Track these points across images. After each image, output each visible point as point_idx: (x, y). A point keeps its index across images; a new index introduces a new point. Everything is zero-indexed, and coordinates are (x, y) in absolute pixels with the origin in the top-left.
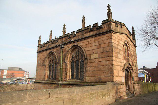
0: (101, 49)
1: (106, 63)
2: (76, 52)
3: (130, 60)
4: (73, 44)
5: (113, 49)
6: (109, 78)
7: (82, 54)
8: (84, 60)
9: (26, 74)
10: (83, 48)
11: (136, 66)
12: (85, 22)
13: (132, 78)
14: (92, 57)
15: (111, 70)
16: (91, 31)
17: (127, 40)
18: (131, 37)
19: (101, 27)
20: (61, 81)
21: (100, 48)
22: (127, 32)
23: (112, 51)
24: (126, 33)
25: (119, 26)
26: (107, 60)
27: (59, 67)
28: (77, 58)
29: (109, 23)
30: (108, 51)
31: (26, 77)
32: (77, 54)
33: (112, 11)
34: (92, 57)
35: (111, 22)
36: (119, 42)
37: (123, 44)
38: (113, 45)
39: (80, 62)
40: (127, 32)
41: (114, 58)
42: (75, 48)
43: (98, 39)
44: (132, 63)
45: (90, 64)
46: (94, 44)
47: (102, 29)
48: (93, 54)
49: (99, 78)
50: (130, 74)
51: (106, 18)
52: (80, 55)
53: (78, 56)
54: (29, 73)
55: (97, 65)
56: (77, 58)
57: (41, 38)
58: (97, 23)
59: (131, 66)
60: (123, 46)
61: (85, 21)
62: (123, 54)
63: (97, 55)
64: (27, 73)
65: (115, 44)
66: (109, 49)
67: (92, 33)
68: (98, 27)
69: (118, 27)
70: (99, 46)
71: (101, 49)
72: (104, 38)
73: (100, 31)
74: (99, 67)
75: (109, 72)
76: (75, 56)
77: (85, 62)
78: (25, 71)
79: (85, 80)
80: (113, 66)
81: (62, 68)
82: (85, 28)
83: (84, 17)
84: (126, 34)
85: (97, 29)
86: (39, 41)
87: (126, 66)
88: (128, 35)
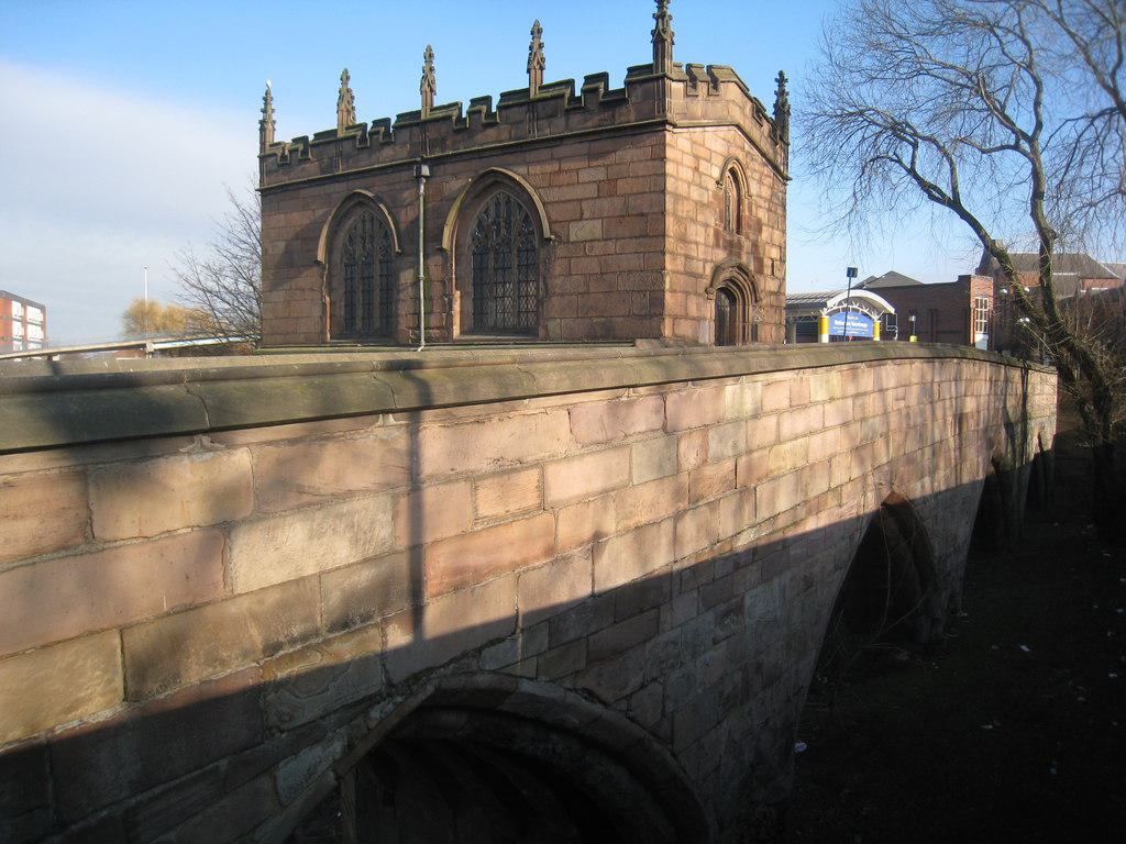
0: (618, 202)
1: (634, 262)
2: (497, 204)
3: (747, 245)
4: (480, 166)
5: (669, 206)
6: (647, 322)
7: (527, 216)
8: (536, 244)
9: (24, 322)
10: (536, 188)
11: (777, 273)
12: (543, 59)
13: (749, 330)
14: (577, 232)
15: (653, 291)
16: (575, 109)
17: (741, 156)
18: (761, 133)
19: (617, 100)
20: (423, 342)
21: (610, 196)
22: (742, 115)
23: (663, 213)
24: (740, 119)
25: (702, 89)
26: (642, 250)
27: (406, 277)
28: (503, 231)
29: (658, 87)
30: (645, 211)
31: (24, 339)
32: (503, 213)
33: (673, 26)
34: (577, 232)
35: (667, 81)
36: (696, 169)
37: (716, 173)
38: (670, 184)
39: (519, 250)
40: (742, 109)
41: (670, 243)
42: (490, 182)
43: (606, 153)
44: (759, 261)
45: (565, 262)
46: (584, 176)
47: (624, 110)
48: (581, 219)
49: (604, 324)
50: (744, 308)
51: (646, 58)
52: (518, 217)
53: (508, 222)
54: (42, 309)
55: (598, 270)
56: (503, 231)
57: (274, 105)
58: (604, 77)
59: (747, 274)
60: (718, 183)
61: (545, 52)
62: (712, 221)
63: (598, 224)
64: (34, 314)
65: (677, 179)
66: (651, 205)
67: (578, 124)
68: (607, 93)
69: (700, 98)
70: (607, 188)
71: (616, 200)
72: (631, 155)
73: (613, 116)
74: (605, 276)
75: (646, 301)
76: (494, 223)
77: (543, 253)
78: (18, 299)
79: (542, 332)
80: (663, 276)
81: (428, 281)
82: (541, 88)
83: (540, 31)
84: (738, 126)
85: (602, 104)
86: (263, 123)
87: (726, 275)
88: (748, 125)
